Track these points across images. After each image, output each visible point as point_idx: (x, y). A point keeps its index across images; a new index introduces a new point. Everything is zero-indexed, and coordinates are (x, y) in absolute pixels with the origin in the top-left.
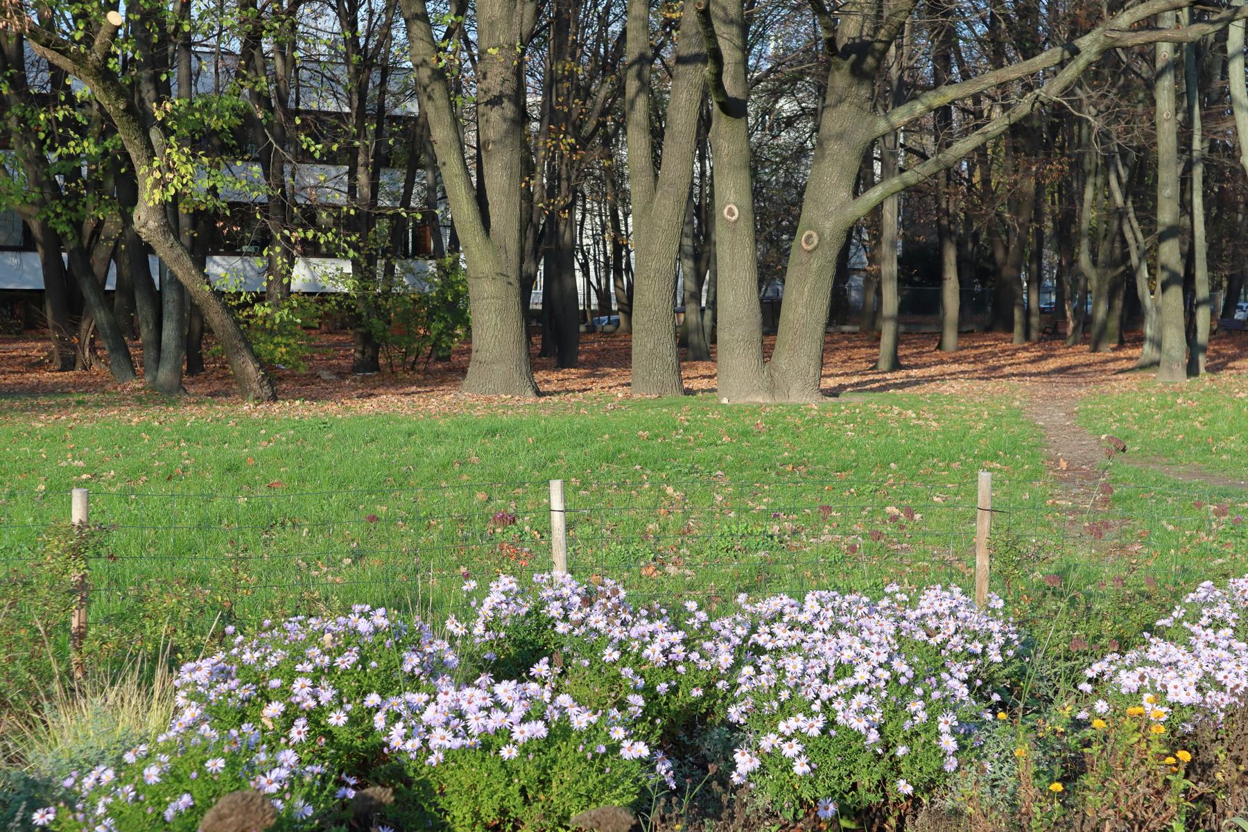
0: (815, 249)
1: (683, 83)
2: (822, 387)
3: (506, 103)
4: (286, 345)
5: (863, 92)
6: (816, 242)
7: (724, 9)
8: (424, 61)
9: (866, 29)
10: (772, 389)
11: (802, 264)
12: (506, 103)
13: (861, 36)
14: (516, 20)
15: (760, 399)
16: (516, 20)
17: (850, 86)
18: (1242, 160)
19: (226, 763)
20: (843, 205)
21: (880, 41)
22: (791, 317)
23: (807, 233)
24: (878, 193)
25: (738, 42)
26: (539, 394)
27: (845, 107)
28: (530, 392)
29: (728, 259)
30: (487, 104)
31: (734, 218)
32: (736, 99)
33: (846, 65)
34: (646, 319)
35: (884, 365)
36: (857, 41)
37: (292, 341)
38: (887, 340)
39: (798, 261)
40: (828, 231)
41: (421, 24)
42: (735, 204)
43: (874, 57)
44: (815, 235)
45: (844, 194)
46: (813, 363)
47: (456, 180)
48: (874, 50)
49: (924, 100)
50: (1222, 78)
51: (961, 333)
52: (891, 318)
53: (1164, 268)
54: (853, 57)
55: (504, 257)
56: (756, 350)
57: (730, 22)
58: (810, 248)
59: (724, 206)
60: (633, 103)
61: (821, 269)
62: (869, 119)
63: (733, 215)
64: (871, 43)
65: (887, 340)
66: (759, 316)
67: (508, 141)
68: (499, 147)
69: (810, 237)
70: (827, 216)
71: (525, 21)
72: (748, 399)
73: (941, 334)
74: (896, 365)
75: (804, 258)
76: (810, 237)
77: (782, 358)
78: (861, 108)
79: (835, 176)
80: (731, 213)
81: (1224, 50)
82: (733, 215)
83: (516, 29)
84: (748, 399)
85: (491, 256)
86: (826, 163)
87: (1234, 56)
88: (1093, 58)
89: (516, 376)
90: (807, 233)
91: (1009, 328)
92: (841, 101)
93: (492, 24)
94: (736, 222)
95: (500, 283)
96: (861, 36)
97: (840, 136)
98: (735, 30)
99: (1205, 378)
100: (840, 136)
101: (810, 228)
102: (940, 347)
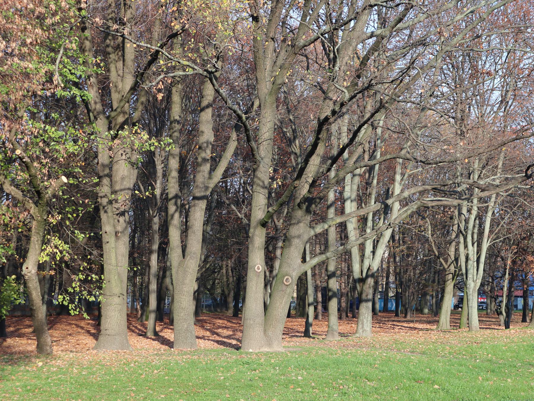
1: (197, 208)
6: (290, 281)
7: (263, 182)
8: (106, 195)
11: (283, 291)
18: (196, 288)
19: (429, 310)
24: (316, 261)
29: (254, 289)
31: (259, 271)
41: (108, 179)
44: (290, 278)
60: (172, 216)
63: (259, 269)
70: (294, 270)
76: (287, 279)
80: (258, 268)
82: (259, 269)
86: (292, 249)
88: (414, 210)
92: (299, 222)
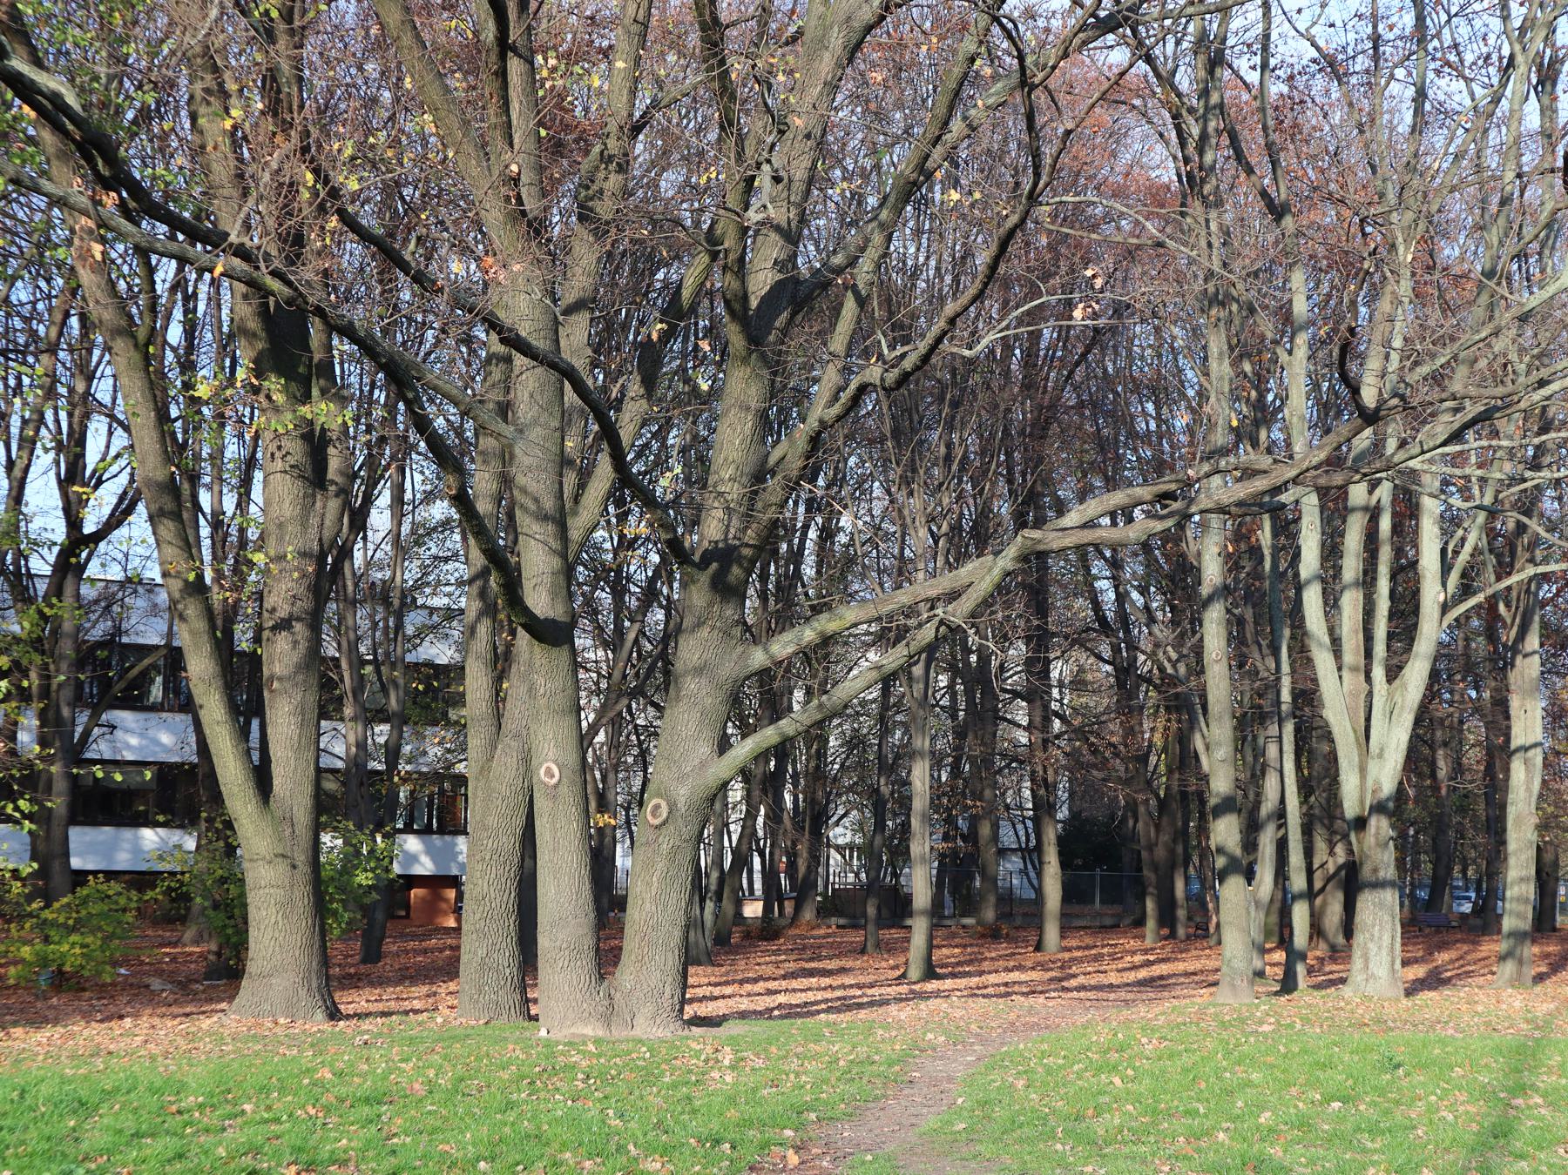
0: (664, 823)
2: (686, 1017)
3: (298, 627)
4: (83, 946)
5: (729, 612)
6: (665, 815)
7: (536, 500)
9: (732, 531)
10: (609, 1015)
12: (298, 627)
13: (726, 539)
14: (314, 521)
15: (588, 1031)
16: (314, 521)
17: (711, 604)
20: (703, 765)
21: (747, 545)
22: (636, 916)
23: (654, 801)
24: (747, 749)
25: (556, 545)
26: (334, 1014)
27: (704, 632)
28: (320, 1015)
30: (273, 628)
32: (554, 621)
33: (704, 578)
34: (478, 916)
35: (915, 973)
36: (721, 545)
37: (89, 940)
38: (919, 938)
39: (643, 840)
40: (683, 800)
42: (555, 762)
43: (740, 565)
44: (664, 804)
45: (705, 749)
46: (670, 979)
47: (218, 729)
48: (740, 556)
49: (815, 624)
50: (155, 396)
51: (1065, 930)
52: (923, 912)
53: (1220, 850)
54: (714, 565)
55: (288, 832)
56: (586, 963)
57: (543, 518)
58: (657, 822)
59: (541, 765)
61: (675, 850)
62: (740, 649)
63: (552, 776)
64: (736, 548)
65: (919, 938)
66: (592, 915)
67: (300, 677)
68: (287, 685)
69: (657, 807)
70: (682, 778)
71: (327, 523)
72: (573, 1030)
73: (1040, 929)
74: (930, 973)
75: (651, 835)
76: (657, 807)
77: (626, 975)
78: (727, 634)
79: (692, 726)
80: (549, 773)
81: (1297, 575)
83: (313, 533)
84: (573, 1030)
85: (269, 831)
87: (1308, 582)
89: (303, 993)
90: (654, 801)
91: (1140, 922)
92: (699, 625)
93: (281, 526)
94: (556, 786)
95: (282, 867)
96: (726, 539)
97: (699, 671)
98: (550, 528)
99: (1305, 995)
100: (699, 671)
101: (659, 795)
102: (1038, 947)
